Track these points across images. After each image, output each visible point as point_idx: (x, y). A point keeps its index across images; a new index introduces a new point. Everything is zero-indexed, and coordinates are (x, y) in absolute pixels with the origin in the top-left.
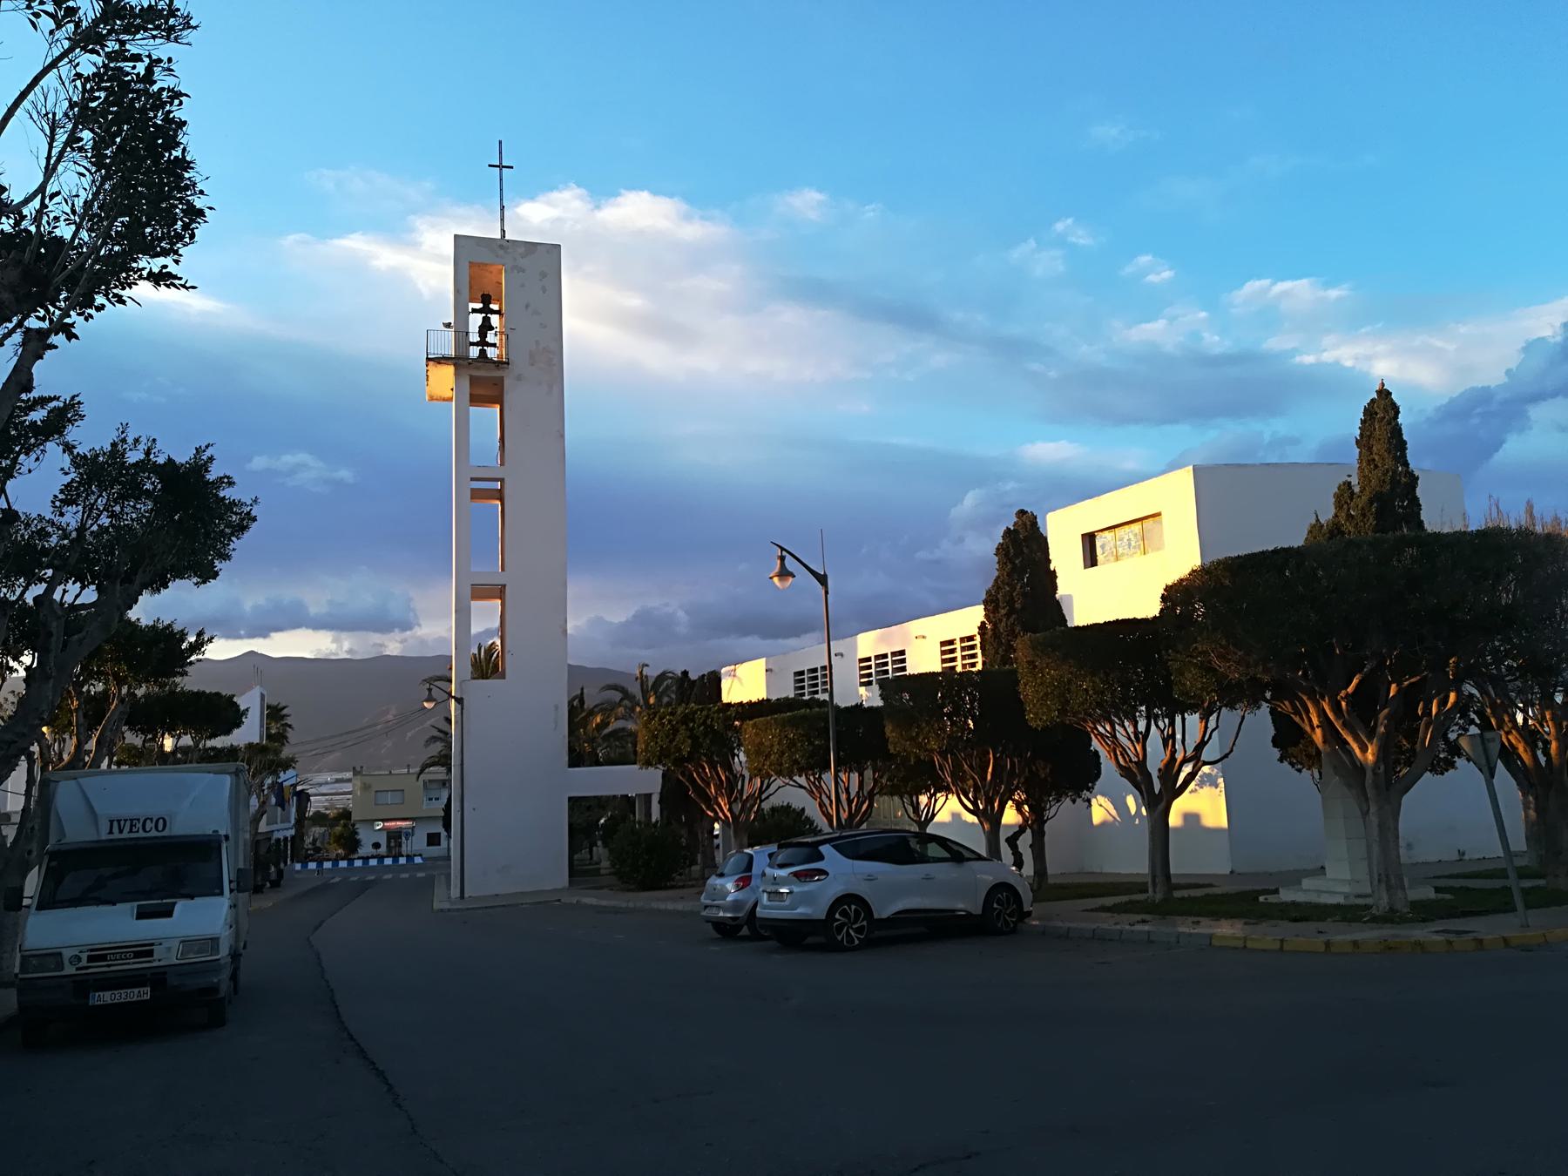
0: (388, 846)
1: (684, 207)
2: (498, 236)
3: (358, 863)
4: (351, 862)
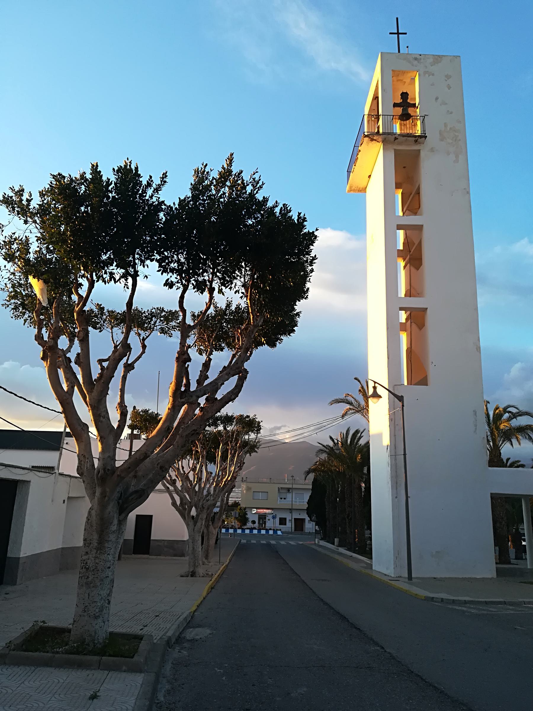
0: (259, 523)
1: (348, 235)
2: (129, 452)
3: (247, 531)
4: (243, 530)
